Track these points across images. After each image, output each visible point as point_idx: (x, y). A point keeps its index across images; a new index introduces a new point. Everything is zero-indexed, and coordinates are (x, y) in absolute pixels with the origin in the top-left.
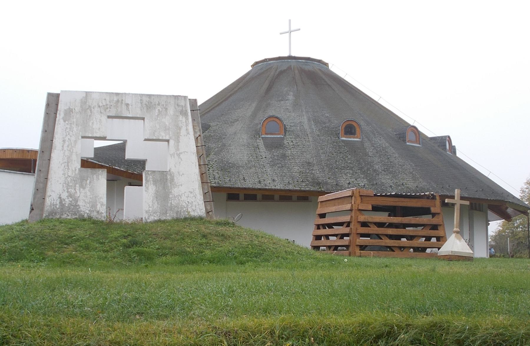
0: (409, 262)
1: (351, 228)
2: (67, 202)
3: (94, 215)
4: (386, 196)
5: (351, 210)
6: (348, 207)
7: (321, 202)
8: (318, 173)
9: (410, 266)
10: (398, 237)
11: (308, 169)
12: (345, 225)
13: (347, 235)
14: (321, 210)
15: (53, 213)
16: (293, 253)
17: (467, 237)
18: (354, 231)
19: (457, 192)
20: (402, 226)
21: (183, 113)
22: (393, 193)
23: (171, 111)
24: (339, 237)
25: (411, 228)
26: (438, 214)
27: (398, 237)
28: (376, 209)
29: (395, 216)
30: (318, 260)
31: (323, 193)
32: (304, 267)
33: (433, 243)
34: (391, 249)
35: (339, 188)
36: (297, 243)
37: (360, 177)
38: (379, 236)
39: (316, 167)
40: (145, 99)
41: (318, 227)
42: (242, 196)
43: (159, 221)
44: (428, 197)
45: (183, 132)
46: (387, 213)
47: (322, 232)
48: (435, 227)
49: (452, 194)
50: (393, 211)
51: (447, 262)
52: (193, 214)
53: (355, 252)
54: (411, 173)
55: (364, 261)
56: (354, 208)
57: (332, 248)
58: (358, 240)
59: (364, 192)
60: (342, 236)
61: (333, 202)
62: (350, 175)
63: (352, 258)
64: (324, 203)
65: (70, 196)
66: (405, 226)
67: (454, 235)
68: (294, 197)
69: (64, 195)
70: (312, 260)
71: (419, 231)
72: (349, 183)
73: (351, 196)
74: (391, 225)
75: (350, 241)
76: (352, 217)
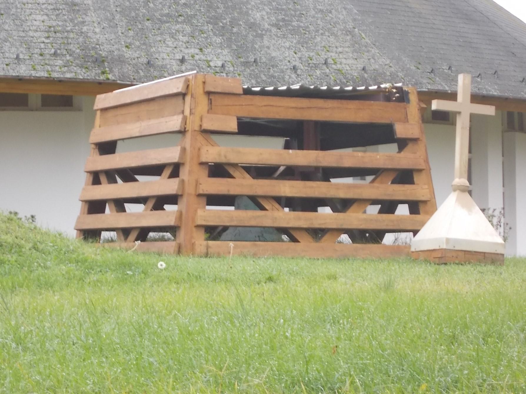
0: (334, 267)
1: (183, 181)
4: (276, 93)
5: (182, 132)
6: (174, 123)
7: (105, 110)
9: (333, 277)
10: (310, 204)
11: (72, 20)
12: (167, 172)
13: (173, 199)
14: (102, 133)
16: (20, 247)
17: (495, 201)
18: (190, 189)
19: (463, 84)
20: (320, 175)
22: (296, 87)
24: (151, 204)
25: (349, 180)
26: (415, 140)
27: (310, 204)
28: (249, 128)
29: (301, 147)
30: (88, 266)
31: (109, 86)
32: (50, 285)
33: (402, 219)
34: (289, 233)
35: (156, 73)
36: (42, 223)
37: (211, 44)
38: (256, 202)
39: (92, 17)
41: (96, 178)
44: (387, 96)
46: (280, 141)
47: (106, 191)
48: (405, 176)
49: (447, 88)
50: (295, 133)
51: (431, 268)
53: (193, 244)
54: (349, 32)
55: (213, 266)
56: (189, 127)
57: (133, 235)
58: (200, 212)
59: (220, 83)
60: (160, 202)
61: (133, 110)
62: (185, 39)
63: (181, 260)
64: (110, 114)
66: (328, 173)
67: (453, 197)
68: (35, 99)
70: (72, 266)
71: (363, 187)
72: (182, 61)
73: (183, 95)
74: (292, 173)
75: (180, 215)
76: (184, 150)
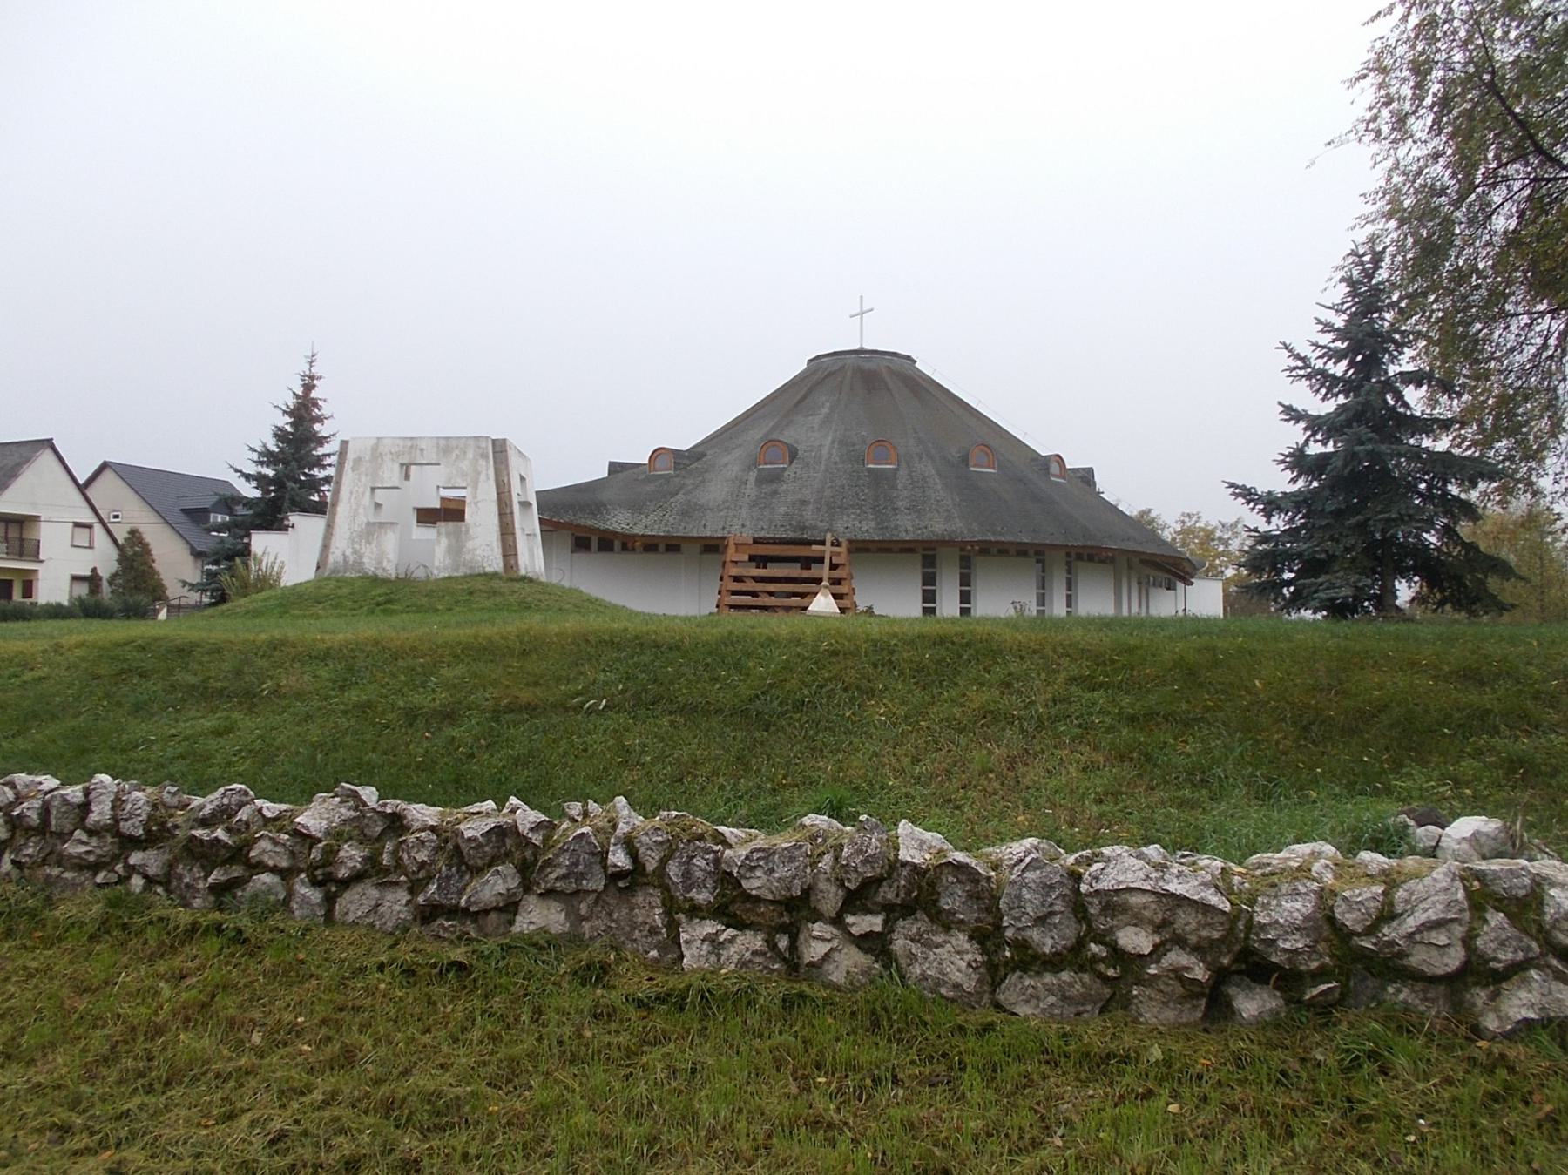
2: (351, 559)
3: (380, 573)
8: (809, 516)
15: (335, 571)
21: (484, 456)
23: (470, 455)
40: (442, 442)
42: (662, 547)
43: (449, 578)
45: (482, 477)
52: (488, 569)
65: (355, 552)
69: (348, 552)
